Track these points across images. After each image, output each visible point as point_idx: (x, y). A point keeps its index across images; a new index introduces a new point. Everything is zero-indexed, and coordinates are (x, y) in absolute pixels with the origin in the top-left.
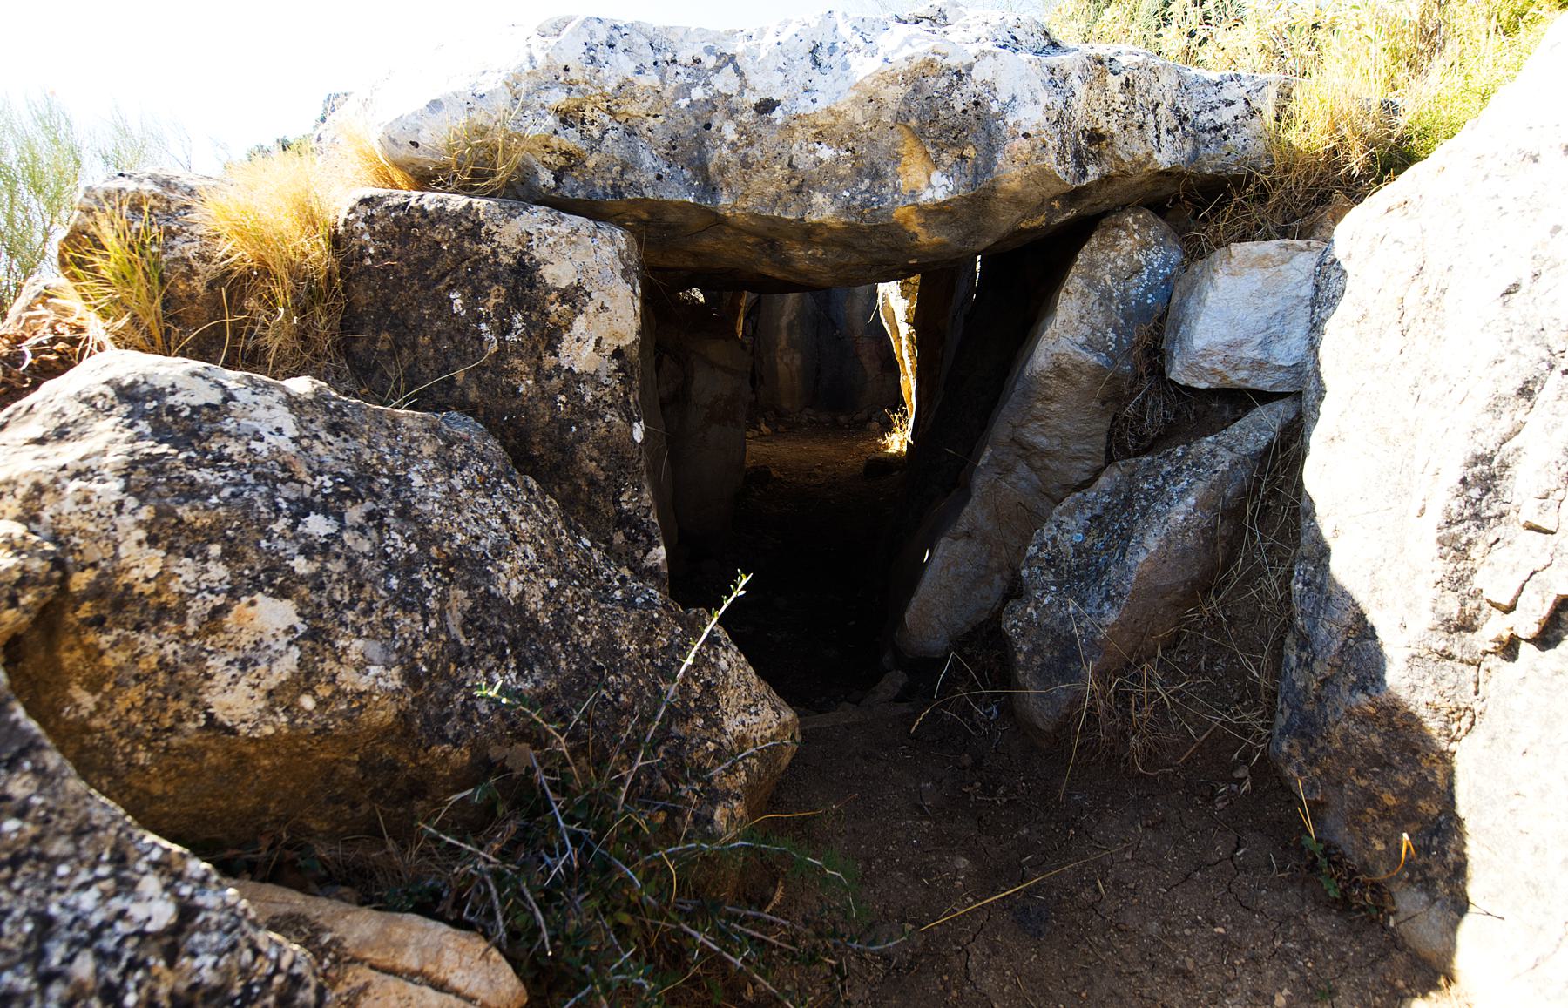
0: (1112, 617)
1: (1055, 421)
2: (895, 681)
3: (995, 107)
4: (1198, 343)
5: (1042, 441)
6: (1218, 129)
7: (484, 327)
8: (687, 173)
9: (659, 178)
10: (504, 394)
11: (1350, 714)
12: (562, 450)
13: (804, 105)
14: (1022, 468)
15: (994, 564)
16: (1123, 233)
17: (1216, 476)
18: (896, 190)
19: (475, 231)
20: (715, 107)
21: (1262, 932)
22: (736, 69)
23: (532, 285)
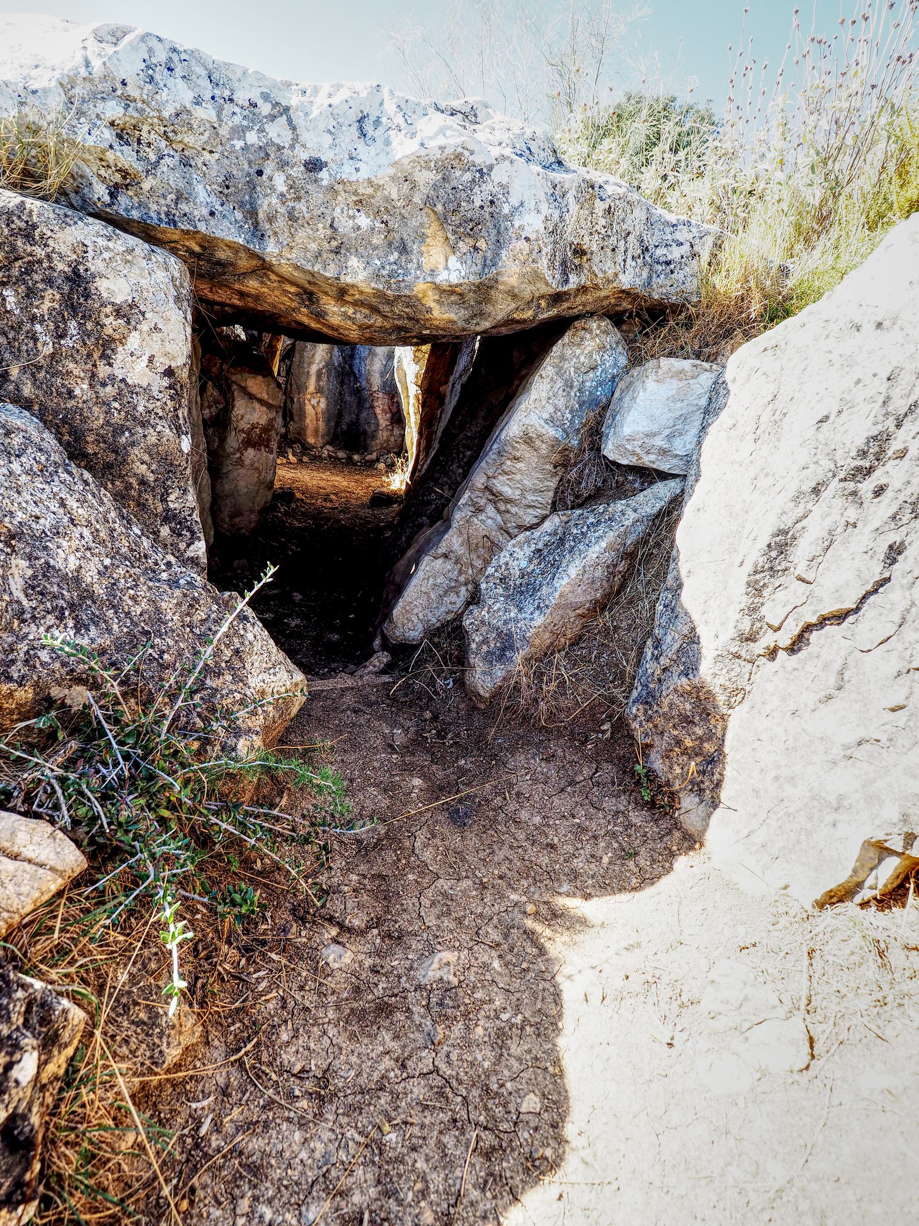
0: (539, 620)
1: (518, 477)
2: (381, 659)
3: (506, 209)
4: (627, 430)
5: (507, 491)
6: (668, 263)
7: (38, 328)
8: (239, 215)
9: (212, 214)
10: (59, 394)
11: (676, 690)
12: (115, 452)
13: (347, 172)
14: (490, 510)
15: (462, 579)
16: (588, 336)
17: (622, 529)
18: (419, 267)
19: (28, 233)
20: (267, 155)
21: (602, 821)
22: (290, 122)
23: (87, 296)
